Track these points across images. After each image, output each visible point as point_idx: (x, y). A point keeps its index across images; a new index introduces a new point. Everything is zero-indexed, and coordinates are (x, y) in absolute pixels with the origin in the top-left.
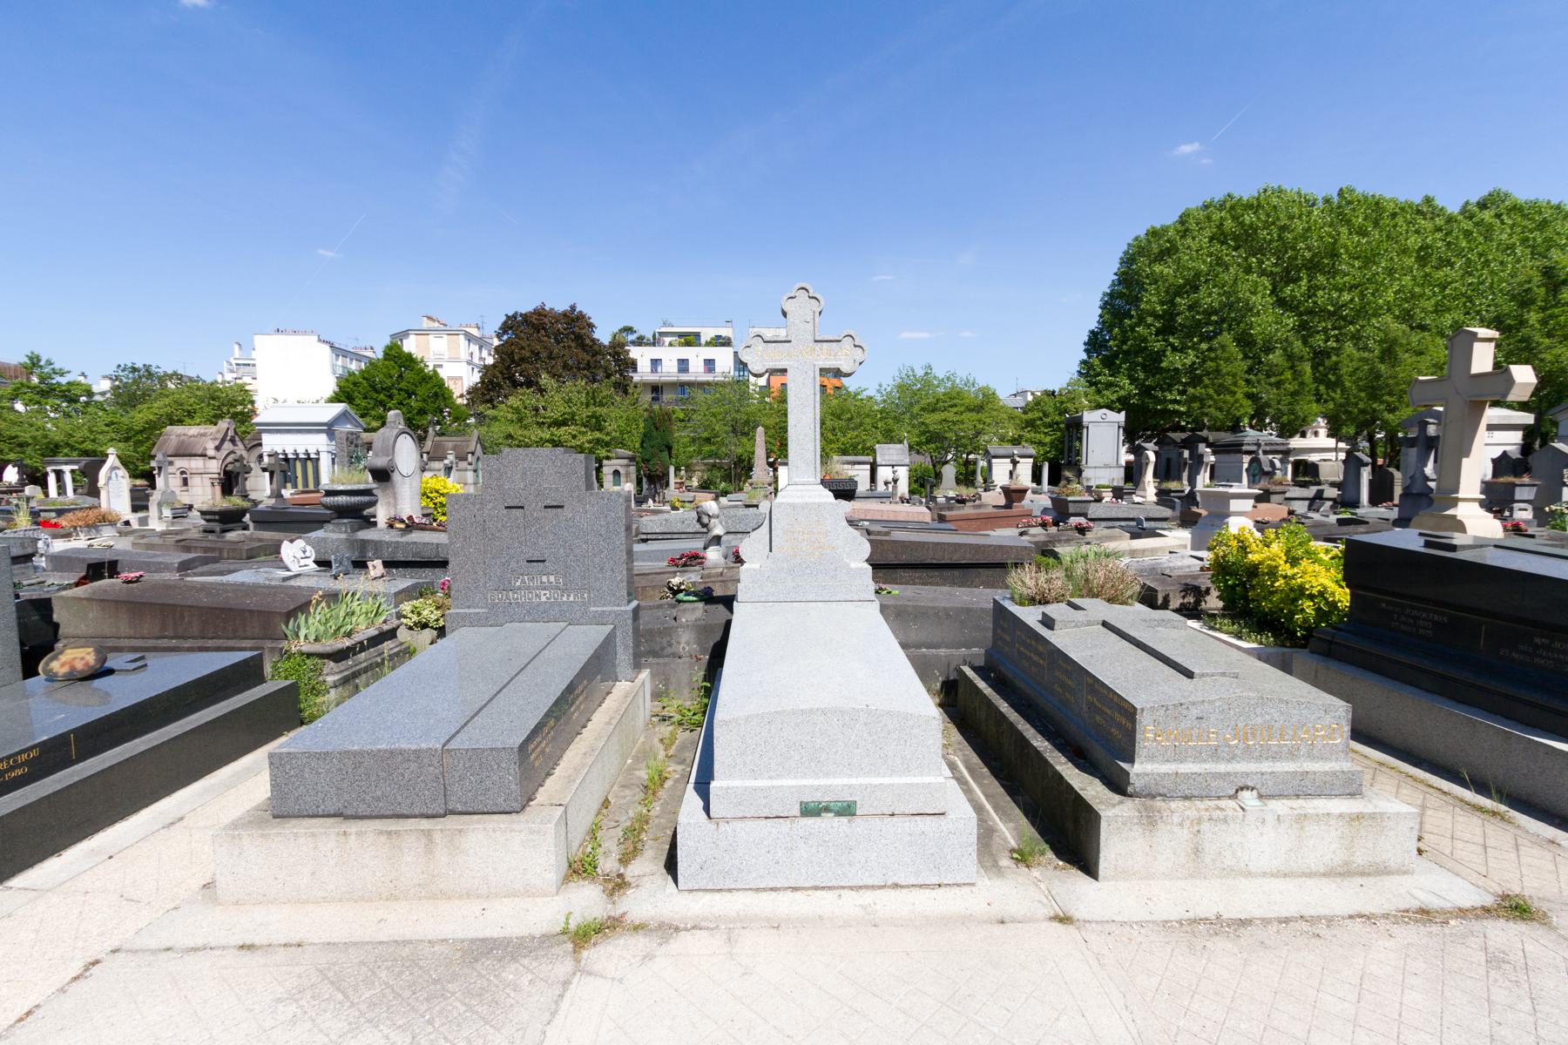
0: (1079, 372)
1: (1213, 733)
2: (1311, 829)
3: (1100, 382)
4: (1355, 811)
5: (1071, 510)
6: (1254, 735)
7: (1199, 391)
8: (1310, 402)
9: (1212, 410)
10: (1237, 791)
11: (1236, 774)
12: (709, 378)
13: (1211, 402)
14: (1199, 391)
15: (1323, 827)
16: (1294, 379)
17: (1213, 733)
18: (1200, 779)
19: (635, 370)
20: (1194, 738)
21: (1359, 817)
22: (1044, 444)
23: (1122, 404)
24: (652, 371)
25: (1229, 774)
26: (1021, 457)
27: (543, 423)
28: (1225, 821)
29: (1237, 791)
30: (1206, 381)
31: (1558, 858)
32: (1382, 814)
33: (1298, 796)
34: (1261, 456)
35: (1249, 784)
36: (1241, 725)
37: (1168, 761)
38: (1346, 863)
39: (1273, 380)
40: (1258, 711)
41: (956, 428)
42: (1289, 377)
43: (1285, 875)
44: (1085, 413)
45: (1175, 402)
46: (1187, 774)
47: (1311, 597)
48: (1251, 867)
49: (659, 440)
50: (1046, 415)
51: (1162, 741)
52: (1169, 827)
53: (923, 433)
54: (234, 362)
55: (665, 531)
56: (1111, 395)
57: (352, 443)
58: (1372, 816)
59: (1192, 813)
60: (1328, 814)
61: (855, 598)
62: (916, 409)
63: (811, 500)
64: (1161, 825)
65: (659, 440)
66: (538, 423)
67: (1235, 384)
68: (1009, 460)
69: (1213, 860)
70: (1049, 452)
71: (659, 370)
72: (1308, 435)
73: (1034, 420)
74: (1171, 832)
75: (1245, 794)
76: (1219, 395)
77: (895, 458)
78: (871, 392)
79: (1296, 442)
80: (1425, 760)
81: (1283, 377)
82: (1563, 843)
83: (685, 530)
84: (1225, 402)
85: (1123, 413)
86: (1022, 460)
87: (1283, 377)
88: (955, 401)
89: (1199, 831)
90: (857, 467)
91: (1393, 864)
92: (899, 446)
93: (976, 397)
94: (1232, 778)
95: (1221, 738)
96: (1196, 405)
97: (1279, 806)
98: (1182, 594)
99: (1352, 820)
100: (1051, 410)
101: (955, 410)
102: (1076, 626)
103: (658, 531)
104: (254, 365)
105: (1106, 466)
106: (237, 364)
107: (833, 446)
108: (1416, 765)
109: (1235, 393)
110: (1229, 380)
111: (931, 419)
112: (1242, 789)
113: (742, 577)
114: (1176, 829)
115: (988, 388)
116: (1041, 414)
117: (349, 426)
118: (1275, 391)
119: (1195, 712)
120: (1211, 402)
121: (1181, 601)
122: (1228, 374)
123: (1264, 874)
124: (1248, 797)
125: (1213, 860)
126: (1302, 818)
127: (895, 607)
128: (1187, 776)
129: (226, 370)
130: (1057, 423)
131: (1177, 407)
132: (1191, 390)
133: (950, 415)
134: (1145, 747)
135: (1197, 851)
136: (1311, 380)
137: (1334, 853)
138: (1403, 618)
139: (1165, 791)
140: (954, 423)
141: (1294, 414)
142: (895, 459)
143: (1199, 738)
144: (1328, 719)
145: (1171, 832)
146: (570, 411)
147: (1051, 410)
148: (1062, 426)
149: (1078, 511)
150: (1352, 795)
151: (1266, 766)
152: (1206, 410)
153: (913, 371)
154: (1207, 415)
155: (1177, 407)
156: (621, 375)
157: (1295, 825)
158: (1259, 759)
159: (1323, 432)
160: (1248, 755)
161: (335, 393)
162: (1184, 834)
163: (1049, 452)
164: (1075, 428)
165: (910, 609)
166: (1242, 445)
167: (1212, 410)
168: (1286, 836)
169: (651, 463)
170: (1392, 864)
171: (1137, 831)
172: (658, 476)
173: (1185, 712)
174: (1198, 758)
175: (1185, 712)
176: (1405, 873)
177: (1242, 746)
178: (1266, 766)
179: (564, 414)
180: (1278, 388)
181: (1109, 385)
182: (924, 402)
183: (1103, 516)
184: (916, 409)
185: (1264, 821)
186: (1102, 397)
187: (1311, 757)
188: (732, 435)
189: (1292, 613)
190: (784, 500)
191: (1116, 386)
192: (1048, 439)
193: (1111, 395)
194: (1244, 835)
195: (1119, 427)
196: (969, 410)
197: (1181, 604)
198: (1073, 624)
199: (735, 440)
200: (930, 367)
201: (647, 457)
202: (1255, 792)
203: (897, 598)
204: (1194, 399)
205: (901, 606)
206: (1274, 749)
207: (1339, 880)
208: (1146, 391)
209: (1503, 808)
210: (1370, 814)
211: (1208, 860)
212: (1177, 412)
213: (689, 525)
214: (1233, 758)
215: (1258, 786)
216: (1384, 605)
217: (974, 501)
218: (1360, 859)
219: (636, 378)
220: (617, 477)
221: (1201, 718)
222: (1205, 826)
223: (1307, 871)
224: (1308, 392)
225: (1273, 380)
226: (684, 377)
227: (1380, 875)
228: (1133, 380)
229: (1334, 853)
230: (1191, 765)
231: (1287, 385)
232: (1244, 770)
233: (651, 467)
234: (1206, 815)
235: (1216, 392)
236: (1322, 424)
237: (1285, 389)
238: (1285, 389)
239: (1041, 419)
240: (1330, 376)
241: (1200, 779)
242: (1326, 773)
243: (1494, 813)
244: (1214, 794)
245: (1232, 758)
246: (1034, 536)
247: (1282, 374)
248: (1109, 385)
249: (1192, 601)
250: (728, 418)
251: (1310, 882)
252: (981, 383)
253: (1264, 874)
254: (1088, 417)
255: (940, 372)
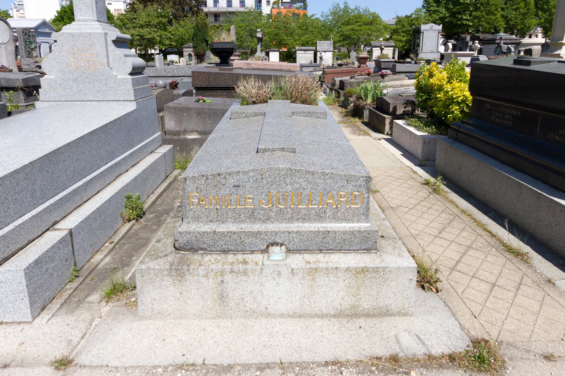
0: (423, 6)
1: (249, 198)
2: (321, 280)
3: (431, 10)
4: (361, 265)
5: (383, 66)
6: (285, 200)
7: (478, 14)
8: (532, 18)
9: (484, 23)
10: (268, 247)
11: (266, 233)
12: (242, 9)
13: (484, 19)
14: (478, 14)
15: (332, 279)
16: (525, 7)
17: (249, 198)
18: (235, 236)
19: (206, 6)
20: (233, 203)
21: (364, 270)
22: (402, 41)
23: (442, 21)
24: (214, 7)
25: (259, 233)
26: (386, 47)
27: (136, 27)
28: (245, 273)
29: (268, 247)
30: (482, 9)
31: (547, 298)
32: (384, 268)
33: (321, 251)
34: (502, 44)
35: (278, 241)
36: (273, 192)
37: (211, 221)
38: (353, 307)
39: (514, 7)
40: (288, 180)
41: (358, 33)
42: (523, 6)
43: (300, 316)
44: (422, 25)
45: (467, 20)
46: (224, 233)
47: (458, 103)
48: (270, 310)
49: (201, 37)
50: (403, 26)
51: (205, 205)
52: (196, 278)
53: (342, 36)
54: (17, 3)
55: (156, 75)
56: (436, 16)
57: (26, 34)
58: (376, 270)
59: (217, 267)
60: (337, 268)
61: (121, 99)
62: (339, 24)
63: (85, 31)
64: (188, 277)
65: (201, 37)
66: (134, 27)
67: (496, 10)
68: (379, 48)
69: (237, 304)
70: (405, 46)
71: (218, 5)
72: (533, 36)
73: (398, 29)
74: (198, 282)
75: (276, 249)
76: (488, 15)
77: (326, 48)
78: (318, 16)
79: (526, 40)
80: (493, 210)
81: (519, 6)
82: (558, 283)
83: (166, 75)
84: (490, 19)
85: (441, 25)
86: (385, 49)
87: (519, 6)
88: (357, 20)
89: (222, 281)
90: (307, 52)
91: (393, 307)
92: (328, 42)
93: (369, 18)
94: (263, 236)
95: (257, 203)
96: (476, 21)
97: (297, 260)
98: (405, 105)
99: (358, 273)
100: (406, 24)
101: (357, 24)
102: (246, 116)
103: (152, 75)
104: (22, 5)
105: (432, 52)
106: (18, 4)
107: (297, 42)
108: (486, 213)
109: (496, 15)
110: (493, 8)
111: (346, 29)
112: (272, 245)
113: (42, 84)
114: (203, 280)
115: (375, 13)
116: (401, 27)
117: (47, 30)
118: (514, 13)
119: (232, 181)
120: (484, 19)
121: (404, 109)
122: (493, 5)
123: (282, 315)
124: (277, 253)
125: (237, 304)
126: (313, 271)
127: (196, 109)
128: (223, 234)
129: (13, 8)
130: (409, 31)
131: (467, 22)
132: (474, 13)
133: (355, 27)
134: (191, 210)
135: (222, 297)
136: (534, 7)
137: (343, 299)
138: (497, 114)
139: (205, 246)
140: (357, 31)
141: (523, 24)
142: (326, 48)
143: (238, 202)
144: (350, 188)
145: (198, 282)
146: (149, 20)
147: (406, 24)
148: (411, 32)
149: (386, 67)
150: (368, 250)
151: (295, 226)
152: (481, 23)
153: (338, 5)
154: (481, 26)
155: (467, 22)
156: (198, 8)
157: (307, 277)
158: (291, 220)
159: (540, 35)
160: (281, 216)
161: (55, 16)
162: (210, 283)
163: (405, 46)
164: (417, 32)
165: (206, 111)
166: (496, 40)
167: (484, 23)
168: (300, 286)
169: (198, 48)
170: (393, 308)
171: (167, 281)
172: (201, 55)
173: (223, 181)
174: (237, 219)
175: (223, 181)
176: (405, 315)
177: (275, 209)
178: (295, 226)
179: (146, 22)
180: (516, 11)
181: (435, 12)
182: (343, 21)
183: (404, 71)
184: (339, 24)
185: (279, 274)
186: (432, 18)
187: (335, 218)
188: (249, 37)
189: (446, 114)
190: (66, 31)
191: (439, 12)
192: (404, 39)
193: (436, 16)
194: (262, 284)
195: (439, 32)
196: (365, 24)
197: (404, 111)
198: (244, 115)
199: (251, 39)
200: (346, 3)
201: (195, 45)
202: (283, 248)
203: (209, 104)
204: (476, 17)
205: (200, 108)
206: (303, 212)
207: (344, 321)
208: (453, 15)
209: (526, 249)
210: (374, 268)
211: (232, 304)
212: (469, 26)
213: (168, 72)
214: (268, 220)
215: (286, 243)
216: (488, 106)
217: (347, 65)
218: (366, 304)
219: (205, 10)
220: (191, 57)
221: (237, 186)
222: (228, 278)
223: (319, 313)
224: (532, 13)
225: (514, 7)
226: (230, 9)
227: (383, 316)
228: (447, 9)
229: (343, 299)
230: (230, 225)
231: (521, 10)
232: (273, 229)
233: (197, 50)
234: (228, 268)
235: (486, 14)
236: (540, 31)
237: (520, 12)
238: (520, 12)
239: (401, 29)
240: (545, 6)
241: (235, 236)
242: (345, 233)
243: (518, 254)
244: (248, 249)
245: (267, 219)
246: (357, 79)
247: (519, 4)
248: (435, 12)
249: (410, 110)
250: (248, 28)
251: (319, 322)
252: (372, 11)
253: (282, 315)
254: (423, 27)
255: (352, 6)
